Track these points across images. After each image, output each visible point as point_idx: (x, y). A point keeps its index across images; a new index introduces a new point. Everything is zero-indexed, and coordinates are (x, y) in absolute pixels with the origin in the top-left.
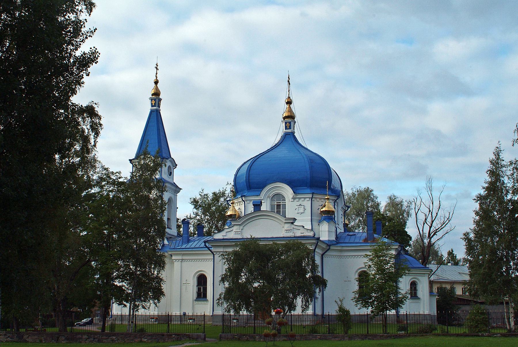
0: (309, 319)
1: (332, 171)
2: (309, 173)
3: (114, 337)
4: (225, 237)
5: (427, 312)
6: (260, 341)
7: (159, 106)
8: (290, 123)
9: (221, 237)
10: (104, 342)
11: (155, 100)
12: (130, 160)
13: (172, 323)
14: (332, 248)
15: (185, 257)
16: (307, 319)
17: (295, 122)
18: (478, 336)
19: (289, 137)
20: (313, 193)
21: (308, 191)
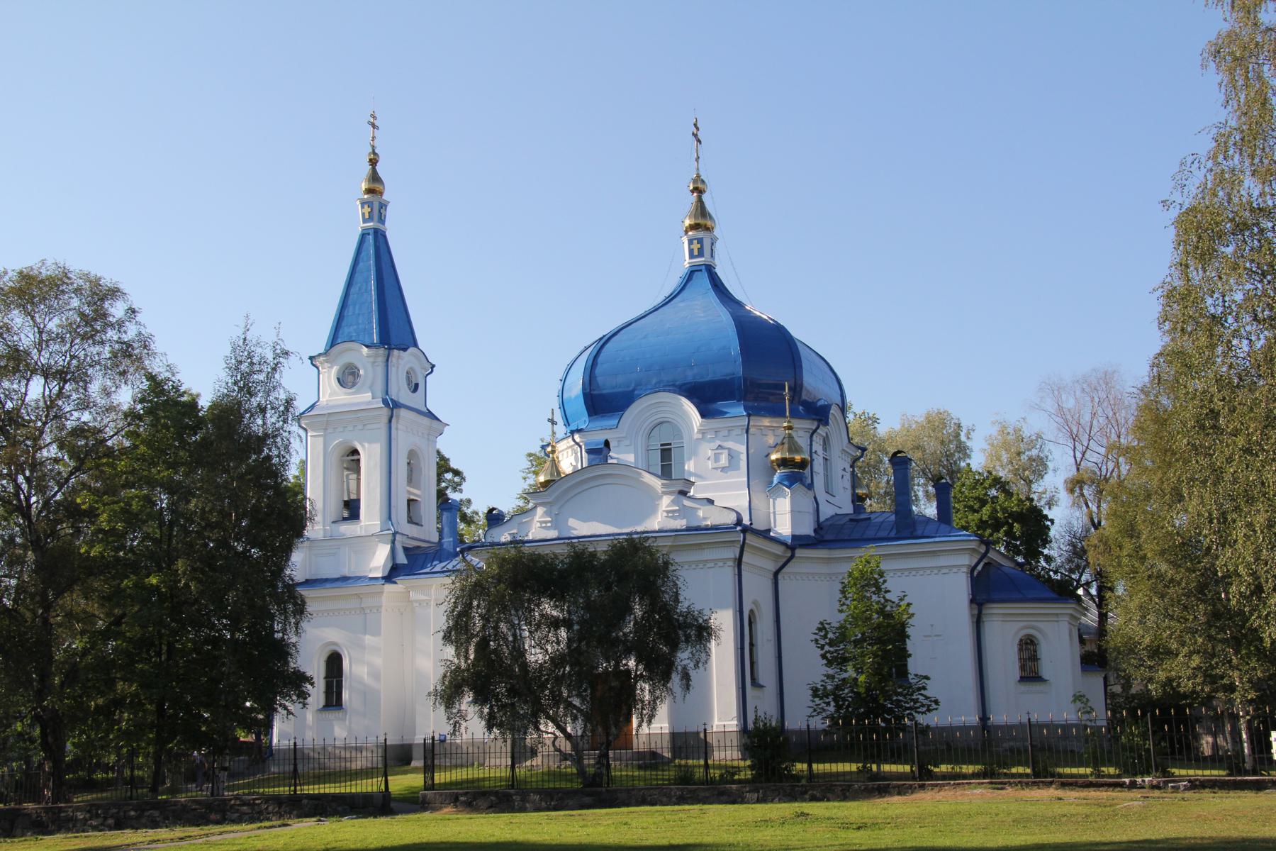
0: (728, 744)
1: (803, 352)
7: (382, 220)
8: (700, 241)
11: (370, 204)
12: (311, 358)
13: (492, 760)
16: (722, 744)
18: (1122, 785)
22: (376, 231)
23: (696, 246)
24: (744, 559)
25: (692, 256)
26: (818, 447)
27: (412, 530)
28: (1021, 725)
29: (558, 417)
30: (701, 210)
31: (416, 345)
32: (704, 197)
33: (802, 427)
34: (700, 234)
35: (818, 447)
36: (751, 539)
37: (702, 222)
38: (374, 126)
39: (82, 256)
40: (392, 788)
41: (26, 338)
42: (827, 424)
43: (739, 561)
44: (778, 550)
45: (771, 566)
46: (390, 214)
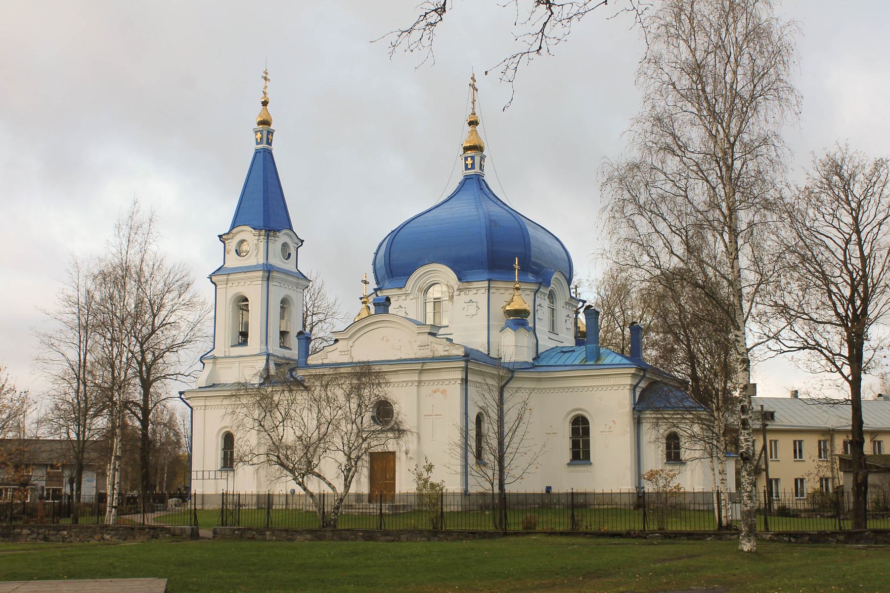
2: (485, 244)
3: (65, 533)
4: (325, 362)
5: (698, 489)
6: (333, 539)
7: (269, 143)
9: (320, 362)
10: (52, 541)
11: (261, 132)
12: (220, 236)
14: (516, 375)
15: (209, 403)
17: (482, 158)
19: (474, 183)
20: (489, 280)
21: (486, 276)
22: (265, 150)
23: (469, 161)
24: (469, 378)
28: (567, 494)
31: (291, 229)
38: (266, 79)
42: (548, 284)
46: (275, 139)
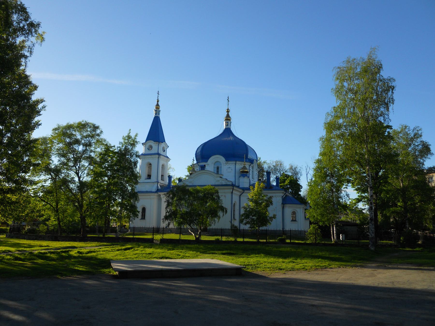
8: (228, 123)
23: (227, 124)
25: (226, 126)
26: (251, 168)
27: (162, 182)
29: (195, 159)
30: (228, 116)
32: (229, 113)
33: (247, 165)
34: (227, 121)
35: (251, 168)
36: (235, 188)
37: (228, 119)
39: (91, 120)
40: (154, 238)
41: (79, 137)
43: (232, 193)
44: (241, 190)
45: (239, 194)
